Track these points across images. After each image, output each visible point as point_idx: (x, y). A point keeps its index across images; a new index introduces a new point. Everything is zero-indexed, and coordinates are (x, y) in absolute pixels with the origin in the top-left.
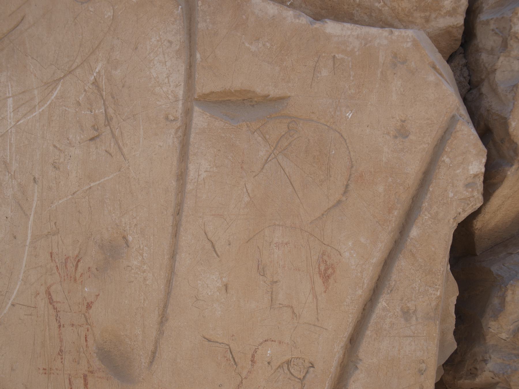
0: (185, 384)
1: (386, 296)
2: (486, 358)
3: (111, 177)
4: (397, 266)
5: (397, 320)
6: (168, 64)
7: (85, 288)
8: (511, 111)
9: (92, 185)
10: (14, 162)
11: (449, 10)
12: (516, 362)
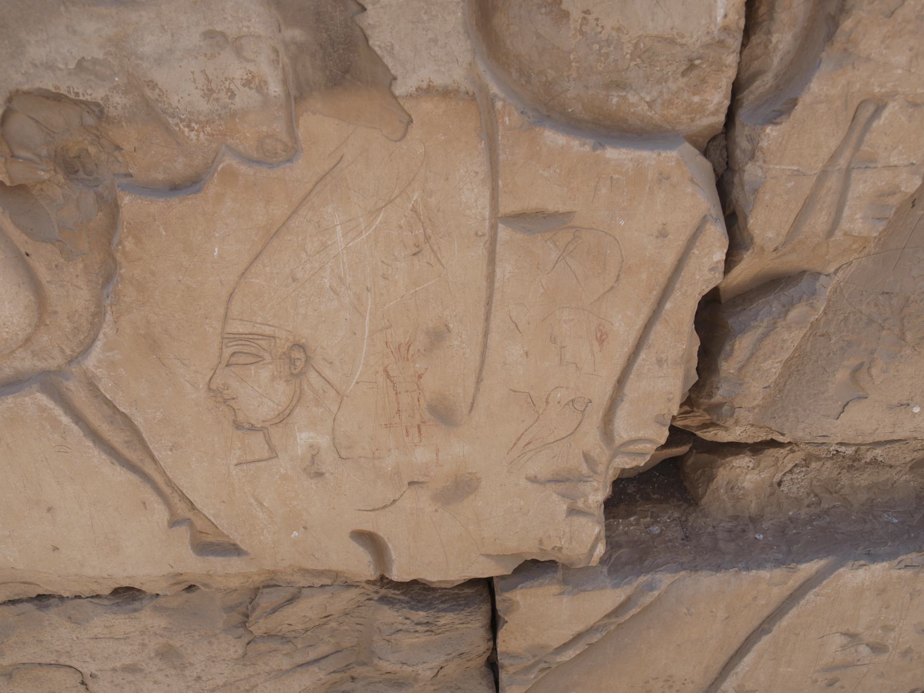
3: (433, 282)
6: (476, 191)
8: (751, 211)
10: (348, 277)
11: (712, 111)
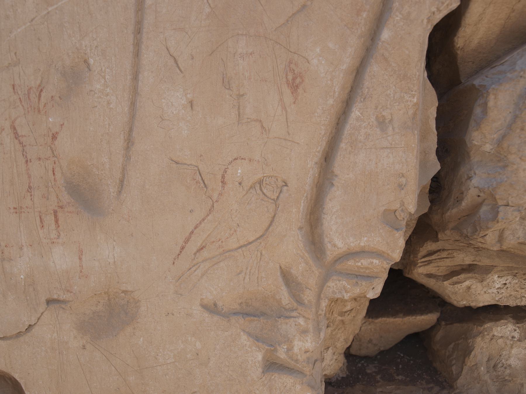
0: (156, 212)
1: (359, 105)
2: (471, 176)
4: (369, 71)
5: (373, 131)
7: (50, 118)
9: (50, 9)
12: (501, 174)
